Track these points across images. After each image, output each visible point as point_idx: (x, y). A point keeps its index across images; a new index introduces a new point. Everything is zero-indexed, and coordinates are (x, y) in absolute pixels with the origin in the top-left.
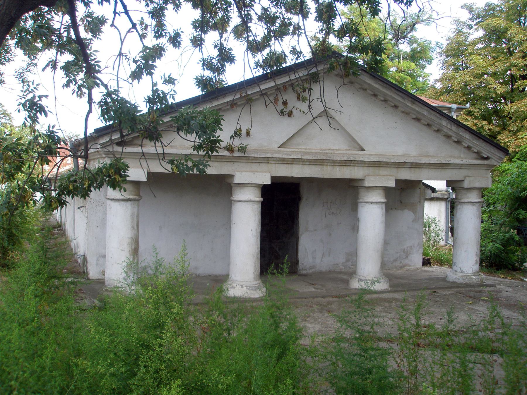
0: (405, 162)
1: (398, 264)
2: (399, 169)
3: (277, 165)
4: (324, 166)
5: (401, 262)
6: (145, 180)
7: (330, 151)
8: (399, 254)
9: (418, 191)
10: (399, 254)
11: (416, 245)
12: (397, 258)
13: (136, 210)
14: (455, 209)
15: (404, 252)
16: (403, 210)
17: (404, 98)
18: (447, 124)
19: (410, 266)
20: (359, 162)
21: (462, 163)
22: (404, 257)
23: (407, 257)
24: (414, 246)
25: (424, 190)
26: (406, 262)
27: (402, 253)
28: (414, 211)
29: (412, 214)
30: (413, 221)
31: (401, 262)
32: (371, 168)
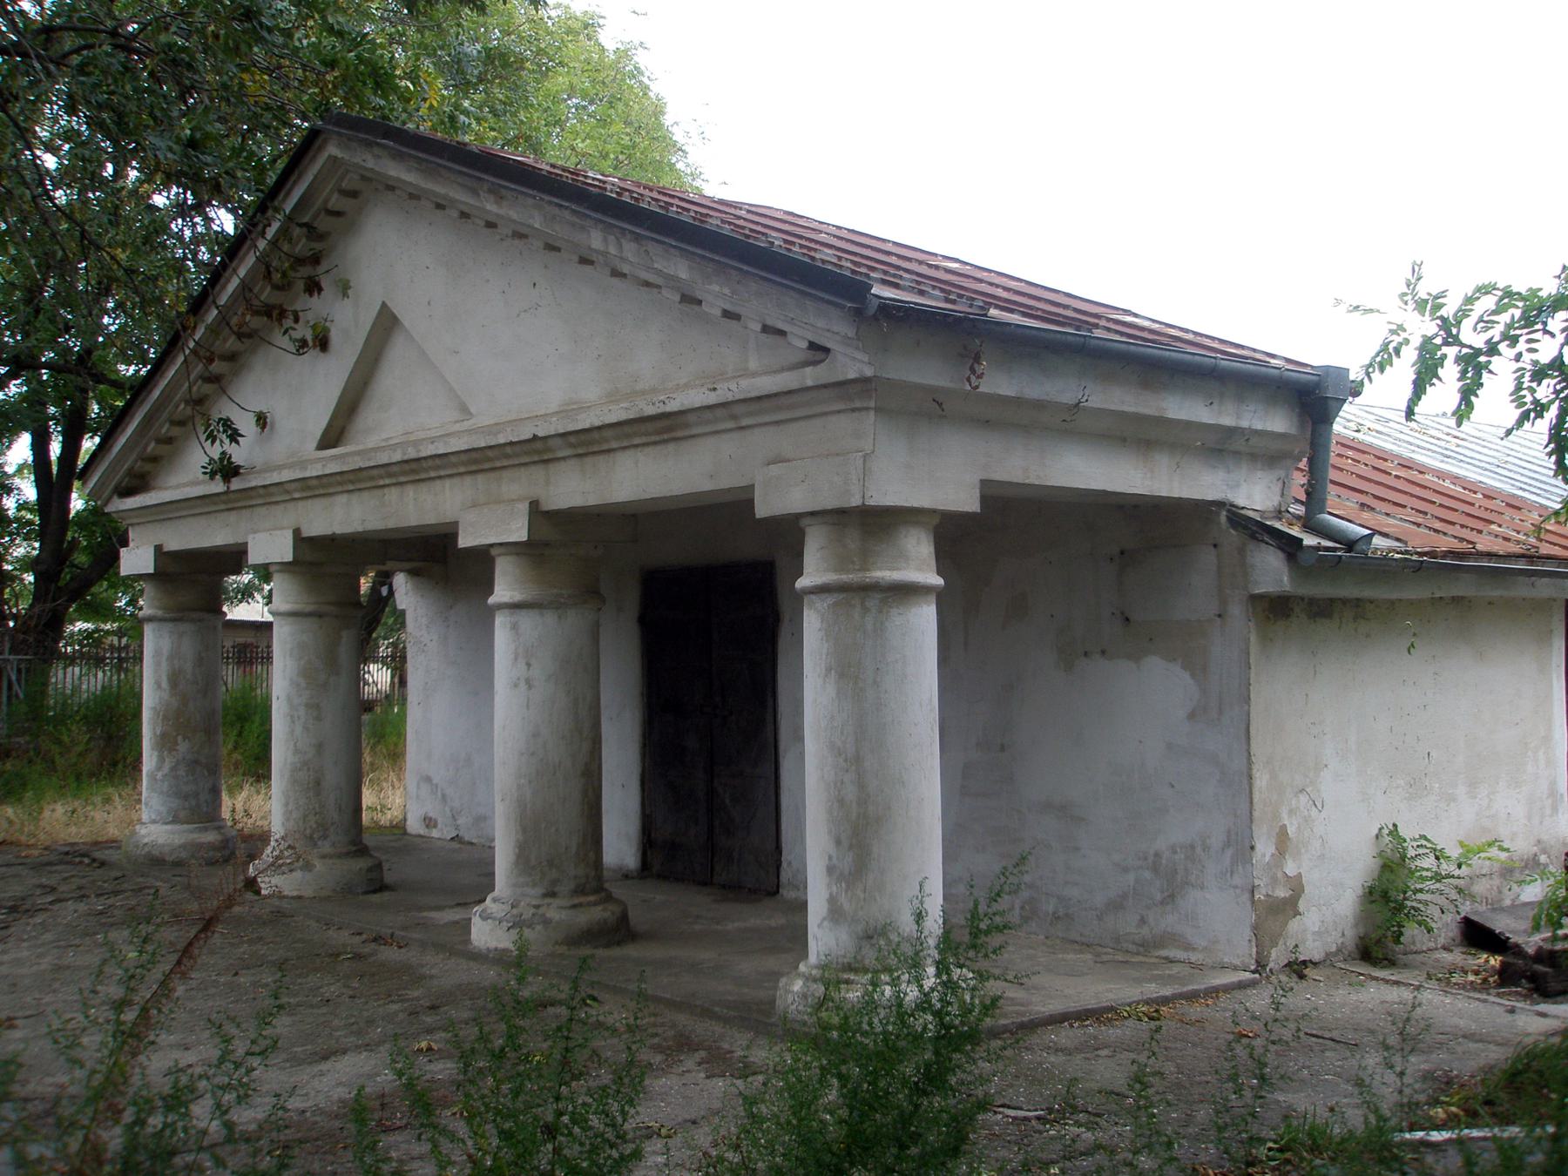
0: (535, 437)
1: (1127, 924)
2: (552, 467)
3: (589, 460)
4: (386, 490)
5: (1143, 921)
6: (123, 573)
7: (637, 441)
8: (1131, 877)
9: (1207, 558)
10: (1131, 877)
11: (1216, 841)
12: (1124, 896)
13: (188, 647)
14: (536, 611)
15: (1155, 869)
16: (1136, 657)
17: (475, 192)
18: (605, 240)
19: (1188, 947)
20: (509, 450)
21: (712, 398)
22: (1159, 897)
23: (1172, 896)
24: (1206, 848)
25: (1242, 551)
26: (1168, 921)
27: (1147, 875)
28: (1196, 665)
29: (1186, 676)
30: (1192, 716)
31: (1143, 921)
32: (480, 478)
